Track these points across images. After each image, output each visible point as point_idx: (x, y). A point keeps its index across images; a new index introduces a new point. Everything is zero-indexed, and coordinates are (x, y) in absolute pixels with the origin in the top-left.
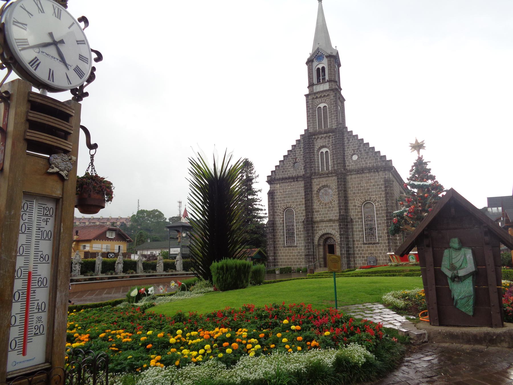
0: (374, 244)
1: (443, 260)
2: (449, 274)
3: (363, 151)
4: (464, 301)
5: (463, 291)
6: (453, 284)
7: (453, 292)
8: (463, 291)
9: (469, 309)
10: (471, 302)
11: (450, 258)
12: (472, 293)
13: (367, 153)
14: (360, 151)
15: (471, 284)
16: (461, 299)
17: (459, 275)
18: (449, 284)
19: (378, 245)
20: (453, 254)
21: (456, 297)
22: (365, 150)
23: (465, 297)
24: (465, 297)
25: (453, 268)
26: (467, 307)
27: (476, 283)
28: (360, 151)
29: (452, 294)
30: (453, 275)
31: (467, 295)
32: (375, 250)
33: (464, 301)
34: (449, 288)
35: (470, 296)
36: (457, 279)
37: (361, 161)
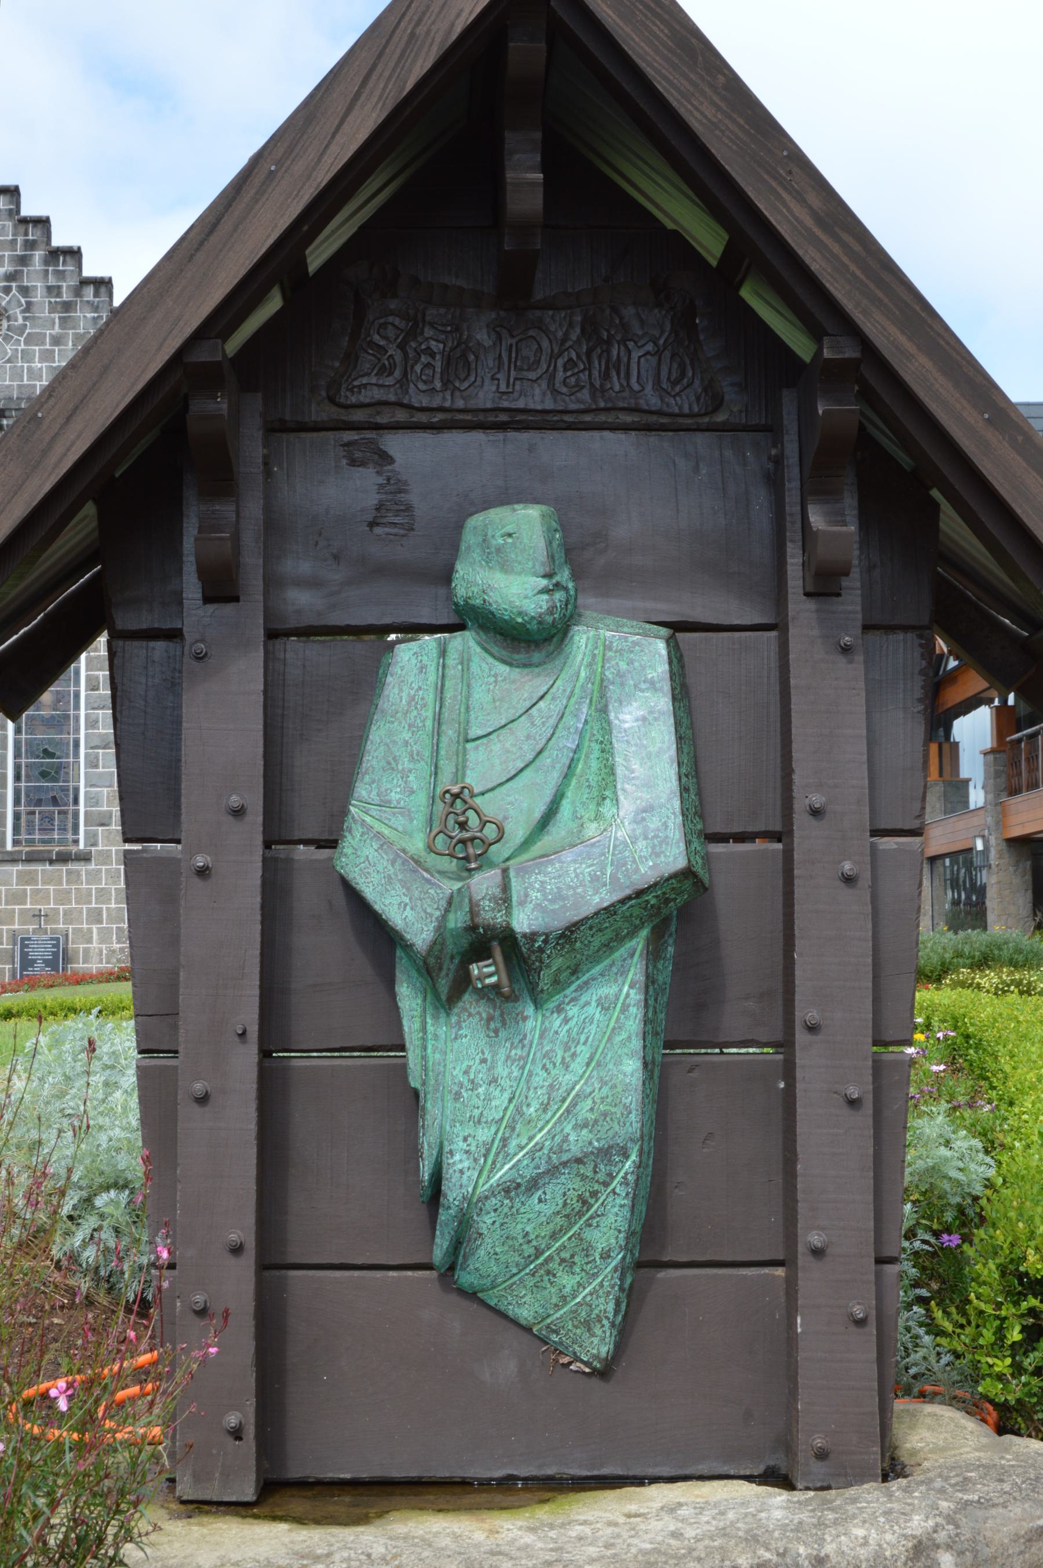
0: (64, 858)
1: (374, 756)
2: (412, 912)
3: (39, 296)
4: (538, 1212)
5: (531, 1106)
6: (439, 1029)
7: (437, 1113)
8: (531, 1106)
9: (579, 1298)
10: (611, 1225)
11: (451, 732)
12: (630, 1121)
13: (67, 306)
14: (25, 291)
15: (633, 1023)
16: (509, 1189)
17: (522, 921)
18: (410, 1027)
19: (82, 868)
20: (480, 695)
21: (463, 1178)
22: (50, 290)
23: (553, 1171)
24: (553, 1171)
25: (463, 835)
26: (568, 1281)
27: (681, 1023)
28: (25, 291)
29: (428, 1143)
30: (457, 920)
31: (578, 1141)
32: (63, 897)
33: (538, 1212)
34: (402, 1070)
35: (605, 1153)
36: (501, 965)
37: (27, 356)
